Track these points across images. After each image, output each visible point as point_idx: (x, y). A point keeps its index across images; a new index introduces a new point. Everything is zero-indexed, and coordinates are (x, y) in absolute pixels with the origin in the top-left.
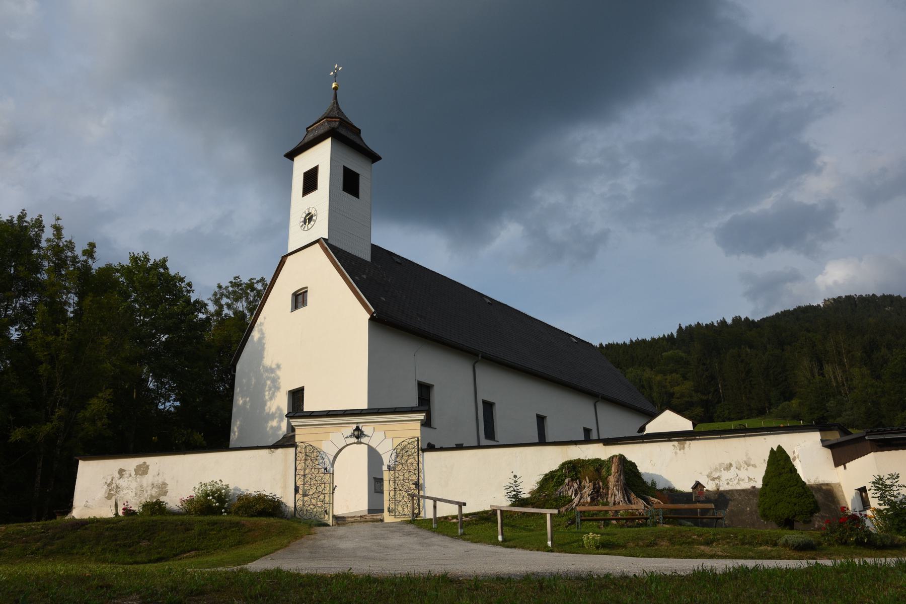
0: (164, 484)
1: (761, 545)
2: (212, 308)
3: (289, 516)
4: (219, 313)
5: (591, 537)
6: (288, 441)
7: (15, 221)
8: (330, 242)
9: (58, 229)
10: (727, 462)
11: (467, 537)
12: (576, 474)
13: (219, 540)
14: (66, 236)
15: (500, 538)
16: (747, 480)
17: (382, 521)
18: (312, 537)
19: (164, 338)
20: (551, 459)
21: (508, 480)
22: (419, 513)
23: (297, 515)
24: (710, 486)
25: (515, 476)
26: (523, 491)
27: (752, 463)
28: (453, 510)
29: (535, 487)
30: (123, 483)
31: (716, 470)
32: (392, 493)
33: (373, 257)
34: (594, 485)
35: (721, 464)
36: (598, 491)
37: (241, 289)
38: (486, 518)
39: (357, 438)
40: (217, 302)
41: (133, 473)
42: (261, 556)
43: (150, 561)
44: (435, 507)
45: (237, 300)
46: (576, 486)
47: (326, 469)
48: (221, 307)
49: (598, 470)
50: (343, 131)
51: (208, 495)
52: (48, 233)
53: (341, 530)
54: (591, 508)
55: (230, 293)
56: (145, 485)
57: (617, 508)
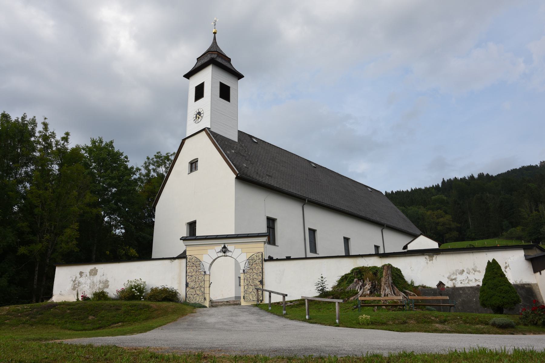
0: (107, 281)
1: (478, 324)
2: (144, 171)
3: (182, 301)
4: (148, 175)
5: (364, 317)
6: (183, 256)
7: (20, 120)
8: (212, 130)
9: (45, 125)
10: (461, 269)
11: (288, 316)
12: (361, 276)
13: (136, 316)
14: (51, 129)
15: (307, 317)
16: (474, 281)
17: (240, 304)
18: (193, 314)
19: (114, 190)
20: (347, 266)
21: (317, 279)
22: (263, 300)
23: (187, 301)
24: (448, 284)
25: (322, 277)
26: (327, 286)
27: (478, 270)
28: (279, 299)
29: (336, 284)
30: (82, 280)
31: (453, 274)
32: (246, 287)
33: (239, 139)
34: (372, 283)
35: (456, 271)
36: (374, 287)
37: (162, 160)
38: (300, 303)
39: (224, 252)
40: (147, 168)
41: (88, 274)
42: (157, 327)
43: (94, 329)
44: (270, 297)
45: (159, 167)
46: (361, 283)
47: (205, 272)
48: (149, 171)
49: (375, 274)
50: (219, 60)
51: (132, 288)
52: (40, 128)
53: (213, 310)
54: (372, 298)
55: (155, 162)
56: (95, 282)
57: (386, 298)
